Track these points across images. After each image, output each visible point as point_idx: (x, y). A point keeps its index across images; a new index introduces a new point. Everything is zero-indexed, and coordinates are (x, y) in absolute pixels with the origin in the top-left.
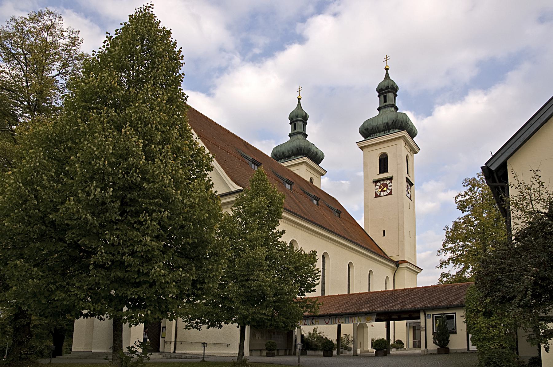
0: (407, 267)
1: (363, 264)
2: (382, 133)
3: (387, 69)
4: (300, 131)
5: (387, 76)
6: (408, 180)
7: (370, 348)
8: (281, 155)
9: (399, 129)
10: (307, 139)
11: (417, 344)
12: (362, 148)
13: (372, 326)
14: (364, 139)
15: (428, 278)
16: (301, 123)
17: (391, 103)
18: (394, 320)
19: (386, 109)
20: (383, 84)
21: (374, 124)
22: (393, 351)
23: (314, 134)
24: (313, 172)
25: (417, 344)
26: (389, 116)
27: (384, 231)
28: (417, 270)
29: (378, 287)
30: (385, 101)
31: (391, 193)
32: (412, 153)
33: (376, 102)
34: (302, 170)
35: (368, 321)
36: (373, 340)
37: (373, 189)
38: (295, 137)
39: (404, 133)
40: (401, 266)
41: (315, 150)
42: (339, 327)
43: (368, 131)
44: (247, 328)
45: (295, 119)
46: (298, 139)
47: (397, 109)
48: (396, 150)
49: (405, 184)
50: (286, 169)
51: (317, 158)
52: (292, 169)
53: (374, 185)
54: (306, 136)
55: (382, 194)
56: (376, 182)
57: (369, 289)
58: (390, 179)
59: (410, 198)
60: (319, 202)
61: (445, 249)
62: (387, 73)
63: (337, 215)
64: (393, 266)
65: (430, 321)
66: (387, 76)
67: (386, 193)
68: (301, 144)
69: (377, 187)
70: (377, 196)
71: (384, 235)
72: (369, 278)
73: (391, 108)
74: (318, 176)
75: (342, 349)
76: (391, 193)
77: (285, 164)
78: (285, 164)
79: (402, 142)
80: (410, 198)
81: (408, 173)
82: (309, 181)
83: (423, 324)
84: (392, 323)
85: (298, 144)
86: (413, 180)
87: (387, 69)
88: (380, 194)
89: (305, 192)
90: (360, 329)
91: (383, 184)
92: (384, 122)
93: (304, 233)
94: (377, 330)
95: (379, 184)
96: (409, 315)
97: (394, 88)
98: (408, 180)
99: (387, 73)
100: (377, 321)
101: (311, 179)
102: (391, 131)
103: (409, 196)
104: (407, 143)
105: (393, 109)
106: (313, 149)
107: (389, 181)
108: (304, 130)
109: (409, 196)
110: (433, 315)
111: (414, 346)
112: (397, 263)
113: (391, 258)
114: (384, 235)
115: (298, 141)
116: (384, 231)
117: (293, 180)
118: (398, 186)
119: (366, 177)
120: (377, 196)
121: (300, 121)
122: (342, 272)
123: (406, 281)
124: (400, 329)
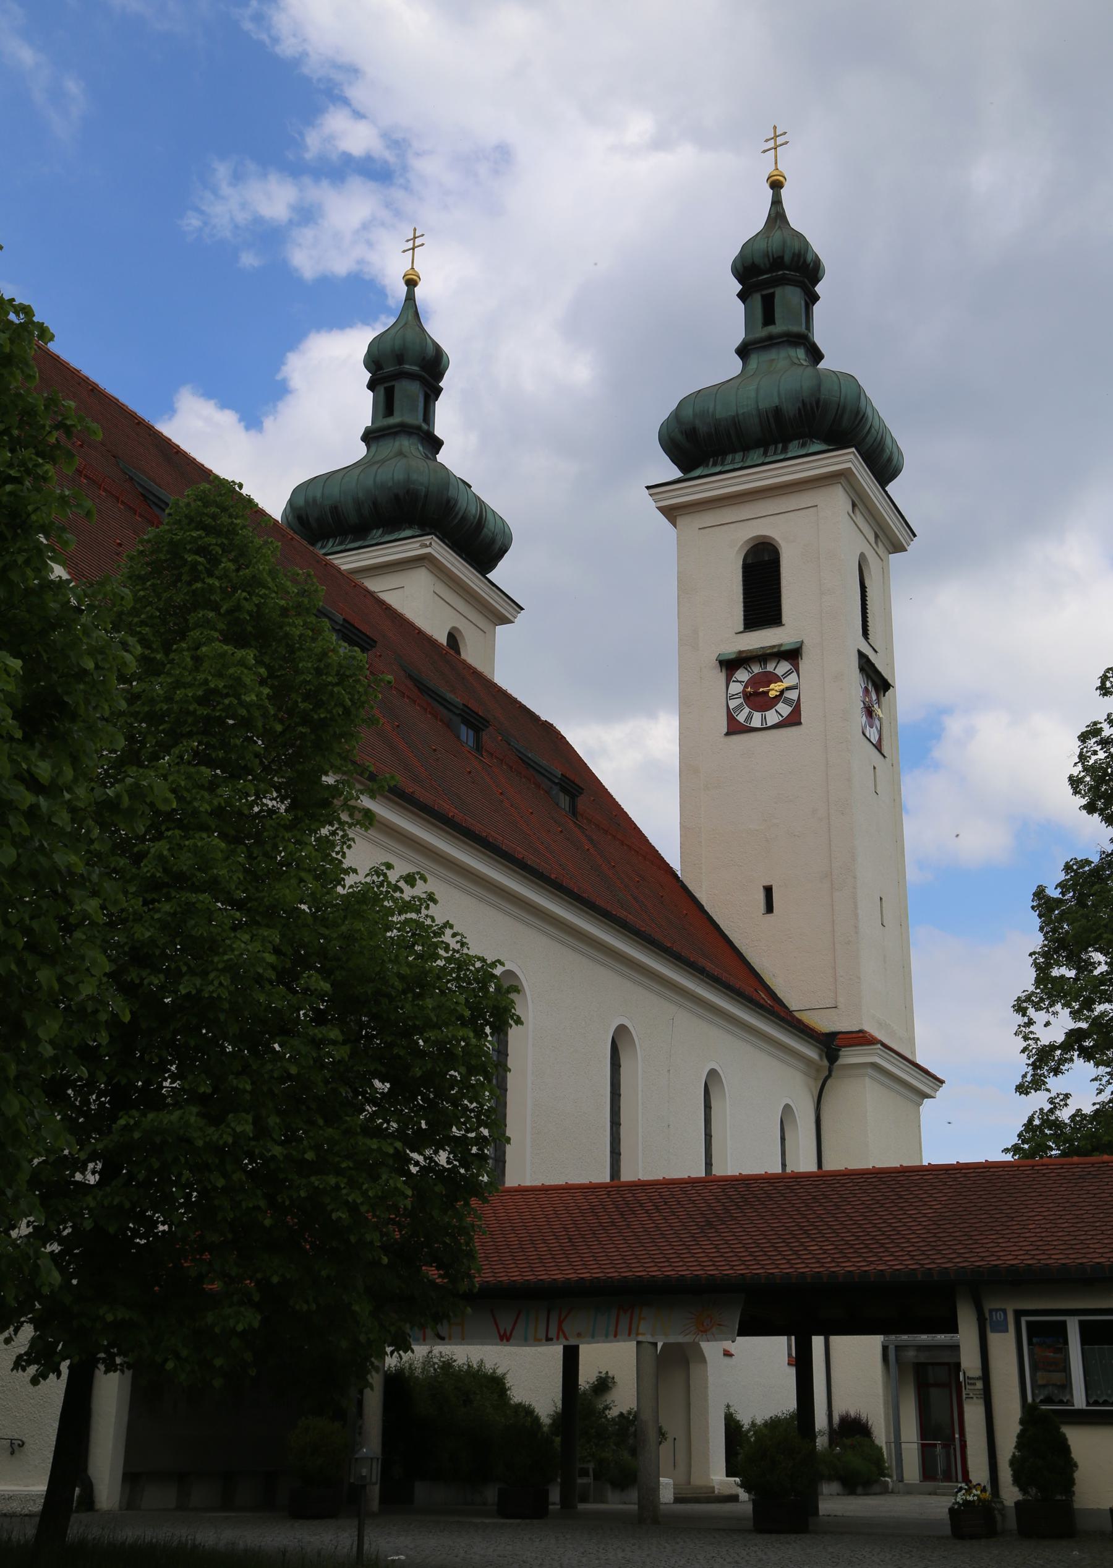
0: (875, 1066)
1: (683, 1043)
2: (756, 456)
3: (776, 185)
4: (410, 419)
5: (777, 216)
6: (867, 667)
7: (717, 1475)
8: (329, 516)
9: (826, 441)
10: (441, 457)
11: (940, 1466)
12: (671, 513)
13: (727, 1354)
14: (679, 474)
15: (972, 1123)
16: (414, 389)
17: (795, 329)
18: (829, 1330)
19: (773, 354)
20: (762, 245)
21: (723, 412)
22: (833, 1503)
23: (465, 441)
24: (460, 605)
25: (940, 1466)
26: (783, 376)
27: (768, 891)
28: (918, 1083)
29: (750, 1150)
30: (769, 318)
31: (794, 720)
32: (881, 550)
33: (731, 320)
34: (416, 594)
35: (706, 1330)
36: (732, 1427)
37: (720, 694)
38: (388, 448)
39: (848, 460)
40: (850, 1057)
41: (473, 509)
42: (571, 1358)
43: (701, 441)
44: (110, 1392)
45: (389, 369)
46: (401, 454)
47: (816, 355)
48: (816, 536)
49: (855, 681)
50: (350, 584)
51: (478, 541)
52: (374, 585)
53: (722, 677)
54: (436, 444)
55: (756, 722)
56: (730, 665)
57: (709, 1164)
58: (793, 655)
59: (878, 747)
60: (485, 737)
61: (1049, 990)
62: (777, 202)
63: (564, 801)
64: (812, 1053)
65: (1004, 1349)
66: (777, 216)
67: (772, 717)
68: (414, 477)
69: (736, 688)
70: (735, 728)
71: (769, 908)
72: (708, 1107)
73: (792, 352)
74: (482, 623)
75: (584, 1473)
76: (794, 720)
77: (347, 562)
78: (347, 562)
79: (837, 500)
80: (878, 747)
81: (865, 633)
82: (443, 640)
83: (970, 1362)
84: (818, 1341)
85: (399, 475)
86: (891, 665)
87: (776, 185)
88: (749, 717)
89: (423, 688)
90: (673, 1366)
91: (757, 680)
92: (762, 406)
93: (751, 648)
94: (750, 1375)
95: (743, 675)
96: (904, 1305)
97: (805, 264)
98: (867, 667)
99: (777, 202)
100: (744, 1331)
101: (453, 638)
102: (794, 448)
103: (873, 735)
104: (859, 502)
105: (801, 353)
106: (462, 503)
107: (783, 667)
108: (428, 415)
109: (873, 735)
110: (1018, 1314)
111: (928, 1472)
112: (831, 1045)
113: (806, 1018)
114: (769, 908)
115: (402, 464)
116: (768, 891)
117: (372, 628)
118: (825, 684)
119: (688, 641)
120: (735, 728)
121: (411, 376)
122: (600, 1088)
123: (868, 1137)
124: (856, 1371)
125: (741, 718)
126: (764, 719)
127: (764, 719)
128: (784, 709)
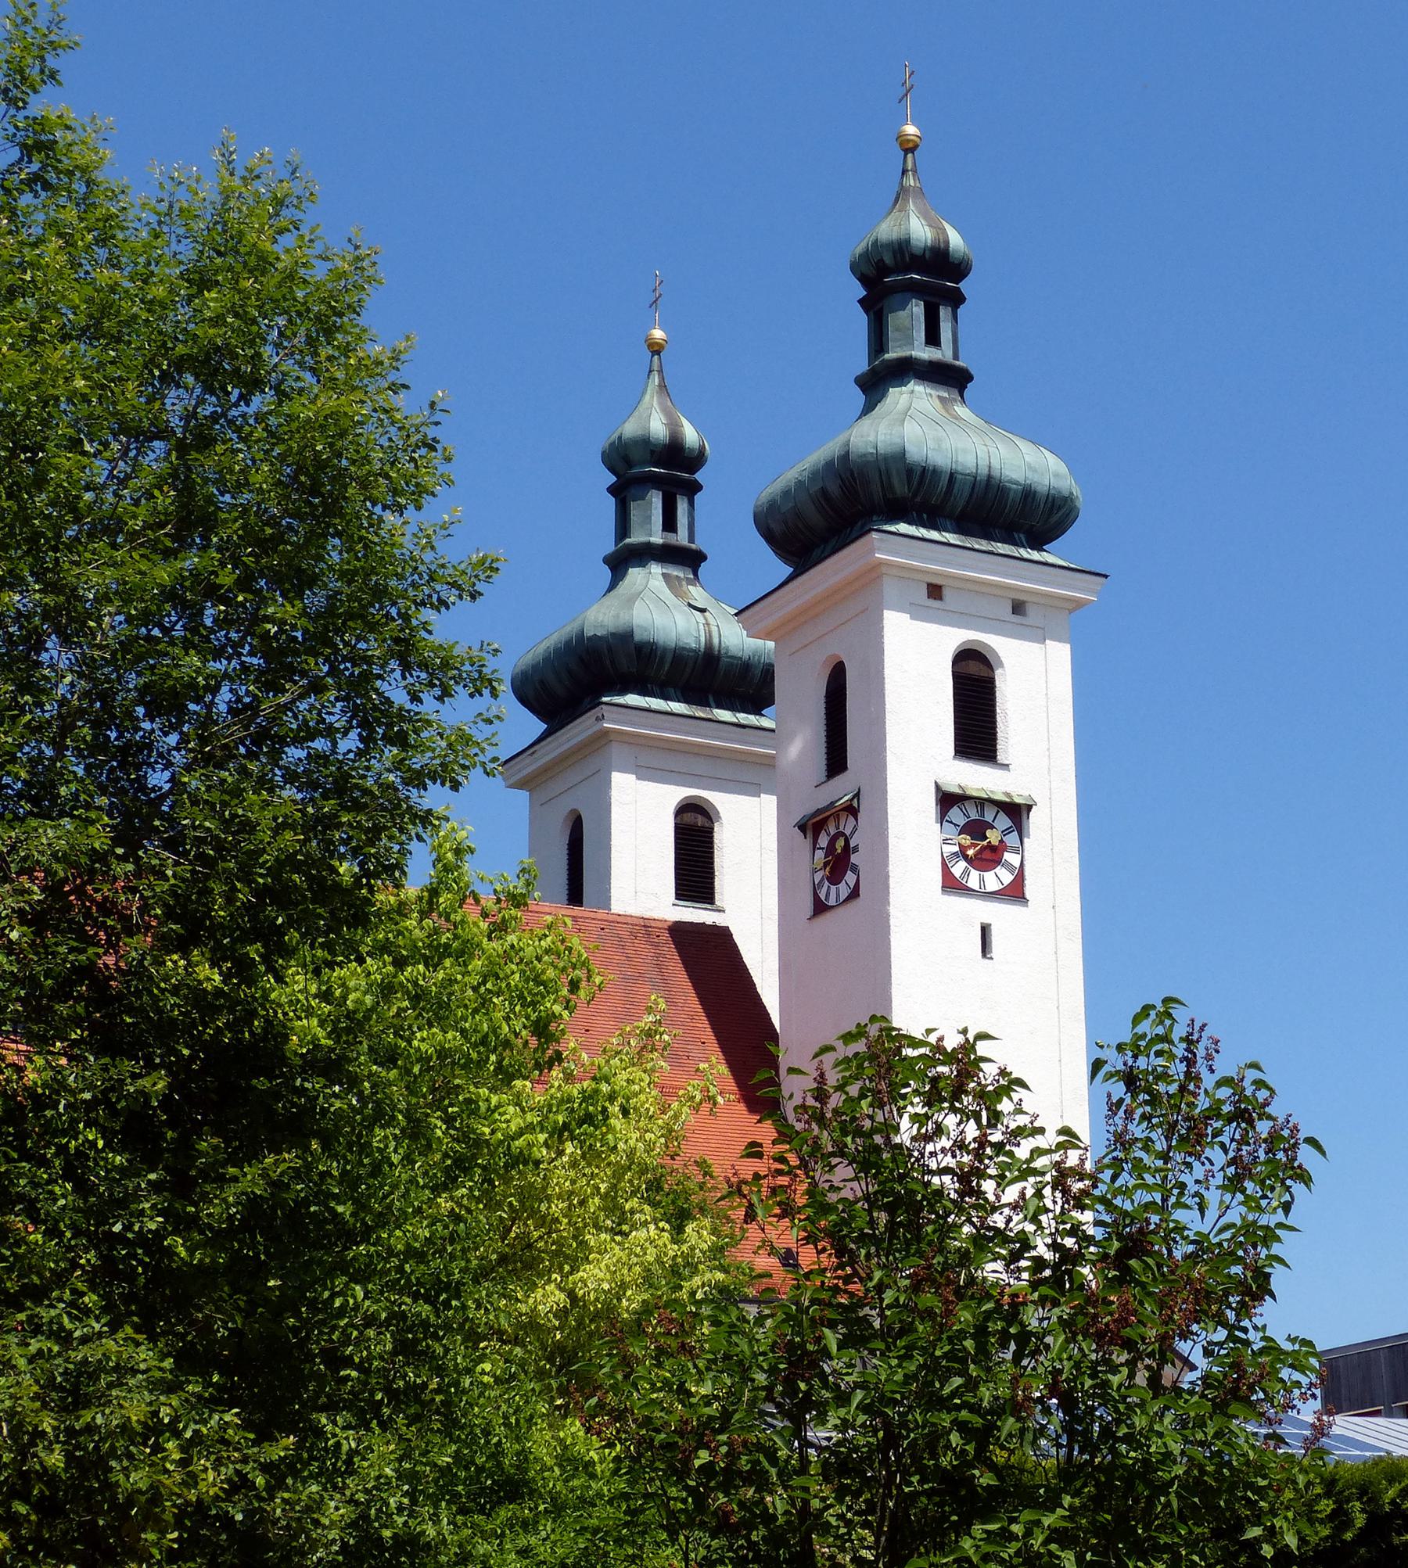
31: (1015, 892)
55: (973, 881)
76: (1015, 892)
95: (956, 815)
125: (958, 868)
126: (982, 880)
127: (982, 880)
128: (1007, 878)
